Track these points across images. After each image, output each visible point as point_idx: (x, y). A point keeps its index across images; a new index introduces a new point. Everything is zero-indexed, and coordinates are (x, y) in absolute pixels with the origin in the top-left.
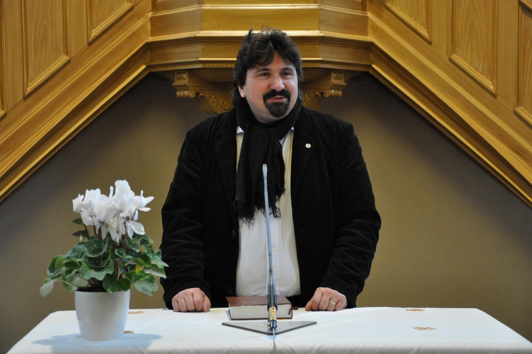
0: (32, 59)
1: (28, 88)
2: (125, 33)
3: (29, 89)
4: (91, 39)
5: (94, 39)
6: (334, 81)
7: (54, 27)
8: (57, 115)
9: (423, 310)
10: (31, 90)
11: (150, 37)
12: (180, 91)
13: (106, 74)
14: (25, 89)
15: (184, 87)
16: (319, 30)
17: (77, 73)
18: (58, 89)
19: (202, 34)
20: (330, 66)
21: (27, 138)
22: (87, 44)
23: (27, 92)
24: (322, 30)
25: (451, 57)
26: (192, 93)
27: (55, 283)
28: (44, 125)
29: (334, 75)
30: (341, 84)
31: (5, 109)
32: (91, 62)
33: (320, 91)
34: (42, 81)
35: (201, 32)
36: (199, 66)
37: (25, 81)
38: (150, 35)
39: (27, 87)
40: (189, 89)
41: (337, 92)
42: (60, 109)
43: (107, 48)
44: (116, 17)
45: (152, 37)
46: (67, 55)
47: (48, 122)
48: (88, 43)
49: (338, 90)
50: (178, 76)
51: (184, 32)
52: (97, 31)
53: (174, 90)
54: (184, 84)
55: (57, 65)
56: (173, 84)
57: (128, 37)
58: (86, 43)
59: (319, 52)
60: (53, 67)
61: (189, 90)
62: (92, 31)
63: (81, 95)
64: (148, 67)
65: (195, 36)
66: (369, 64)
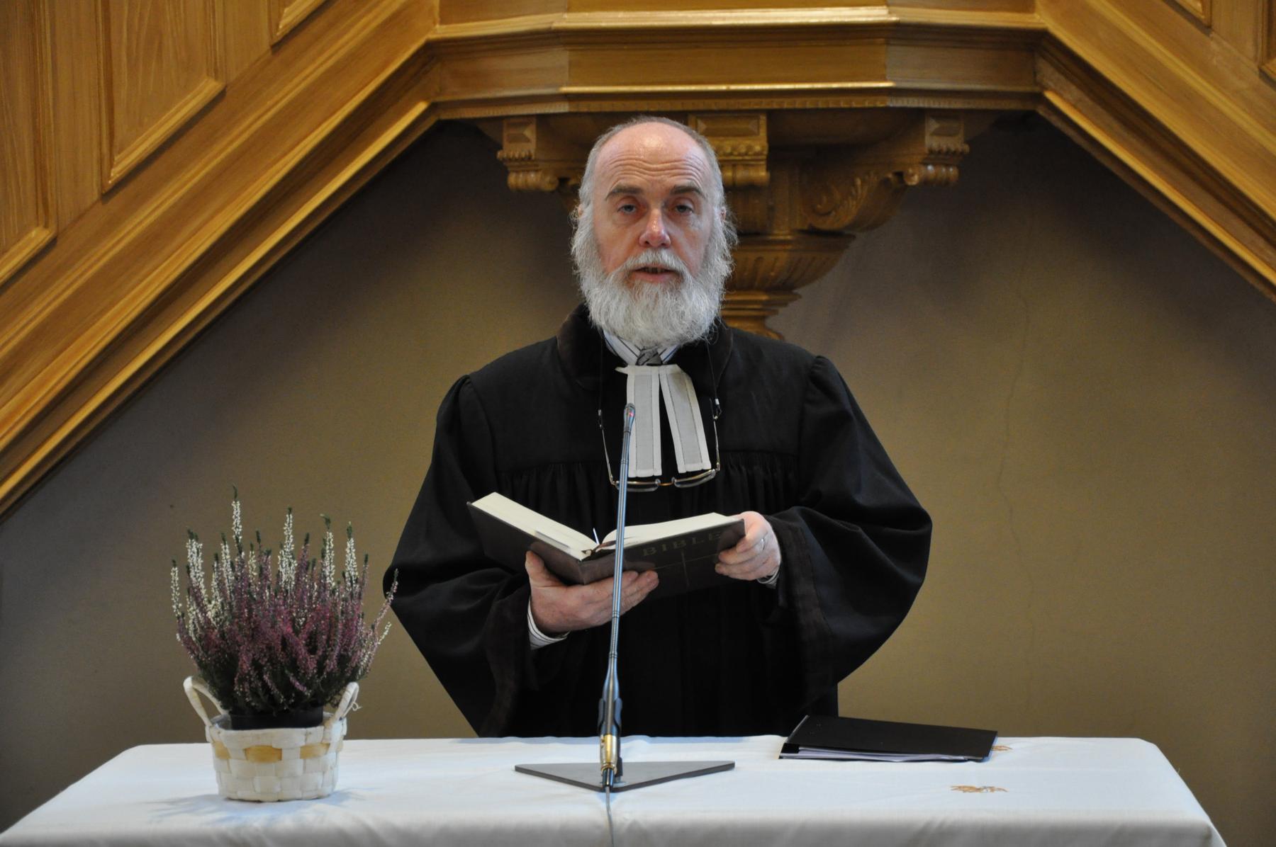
0: (121, 94)
1: (113, 170)
2: (370, 16)
3: (116, 173)
4: (279, 35)
5: (287, 32)
6: (932, 141)
7: (182, 6)
8: (189, 242)
10: (121, 174)
11: (438, 26)
12: (517, 172)
13: (320, 129)
15: (526, 163)
16: (888, 5)
17: (241, 128)
19: (569, 22)
20: (919, 103)
21: (113, 304)
22: (269, 48)
23: (110, 179)
24: (894, 5)
25: (1264, 68)
26: (548, 179)
28: (156, 268)
29: (933, 125)
30: (953, 149)
31: (53, 227)
32: (280, 95)
33: (897, 170)
34: (151, 150)
35: (566, 16)
36: (563, 108)
37: (105, 150)
38: (439, 19)
39: (111, 166)
40: (539, 168)
41: (944, 170)
43: (321, 59)
44: (31, 251)
45: (444, 27)
46: (216, 78)
47: (166, 259)
48: (272, 43)
49: (947, 166)
50: (513, 132)
51: (524, 15)
52: (297, 12)
53: (502, 169)
54: (526, 155)
55: (190, 105)
56: (499, 154)
57: (378, 26)
58: (265, 45)
59: (885, 67)
60: (178, 111)
61: (540, 170)
62: (283, 10)
63: (256, 184)
64: (433, 108)
65: (550, 28)
66: (1037, 89)
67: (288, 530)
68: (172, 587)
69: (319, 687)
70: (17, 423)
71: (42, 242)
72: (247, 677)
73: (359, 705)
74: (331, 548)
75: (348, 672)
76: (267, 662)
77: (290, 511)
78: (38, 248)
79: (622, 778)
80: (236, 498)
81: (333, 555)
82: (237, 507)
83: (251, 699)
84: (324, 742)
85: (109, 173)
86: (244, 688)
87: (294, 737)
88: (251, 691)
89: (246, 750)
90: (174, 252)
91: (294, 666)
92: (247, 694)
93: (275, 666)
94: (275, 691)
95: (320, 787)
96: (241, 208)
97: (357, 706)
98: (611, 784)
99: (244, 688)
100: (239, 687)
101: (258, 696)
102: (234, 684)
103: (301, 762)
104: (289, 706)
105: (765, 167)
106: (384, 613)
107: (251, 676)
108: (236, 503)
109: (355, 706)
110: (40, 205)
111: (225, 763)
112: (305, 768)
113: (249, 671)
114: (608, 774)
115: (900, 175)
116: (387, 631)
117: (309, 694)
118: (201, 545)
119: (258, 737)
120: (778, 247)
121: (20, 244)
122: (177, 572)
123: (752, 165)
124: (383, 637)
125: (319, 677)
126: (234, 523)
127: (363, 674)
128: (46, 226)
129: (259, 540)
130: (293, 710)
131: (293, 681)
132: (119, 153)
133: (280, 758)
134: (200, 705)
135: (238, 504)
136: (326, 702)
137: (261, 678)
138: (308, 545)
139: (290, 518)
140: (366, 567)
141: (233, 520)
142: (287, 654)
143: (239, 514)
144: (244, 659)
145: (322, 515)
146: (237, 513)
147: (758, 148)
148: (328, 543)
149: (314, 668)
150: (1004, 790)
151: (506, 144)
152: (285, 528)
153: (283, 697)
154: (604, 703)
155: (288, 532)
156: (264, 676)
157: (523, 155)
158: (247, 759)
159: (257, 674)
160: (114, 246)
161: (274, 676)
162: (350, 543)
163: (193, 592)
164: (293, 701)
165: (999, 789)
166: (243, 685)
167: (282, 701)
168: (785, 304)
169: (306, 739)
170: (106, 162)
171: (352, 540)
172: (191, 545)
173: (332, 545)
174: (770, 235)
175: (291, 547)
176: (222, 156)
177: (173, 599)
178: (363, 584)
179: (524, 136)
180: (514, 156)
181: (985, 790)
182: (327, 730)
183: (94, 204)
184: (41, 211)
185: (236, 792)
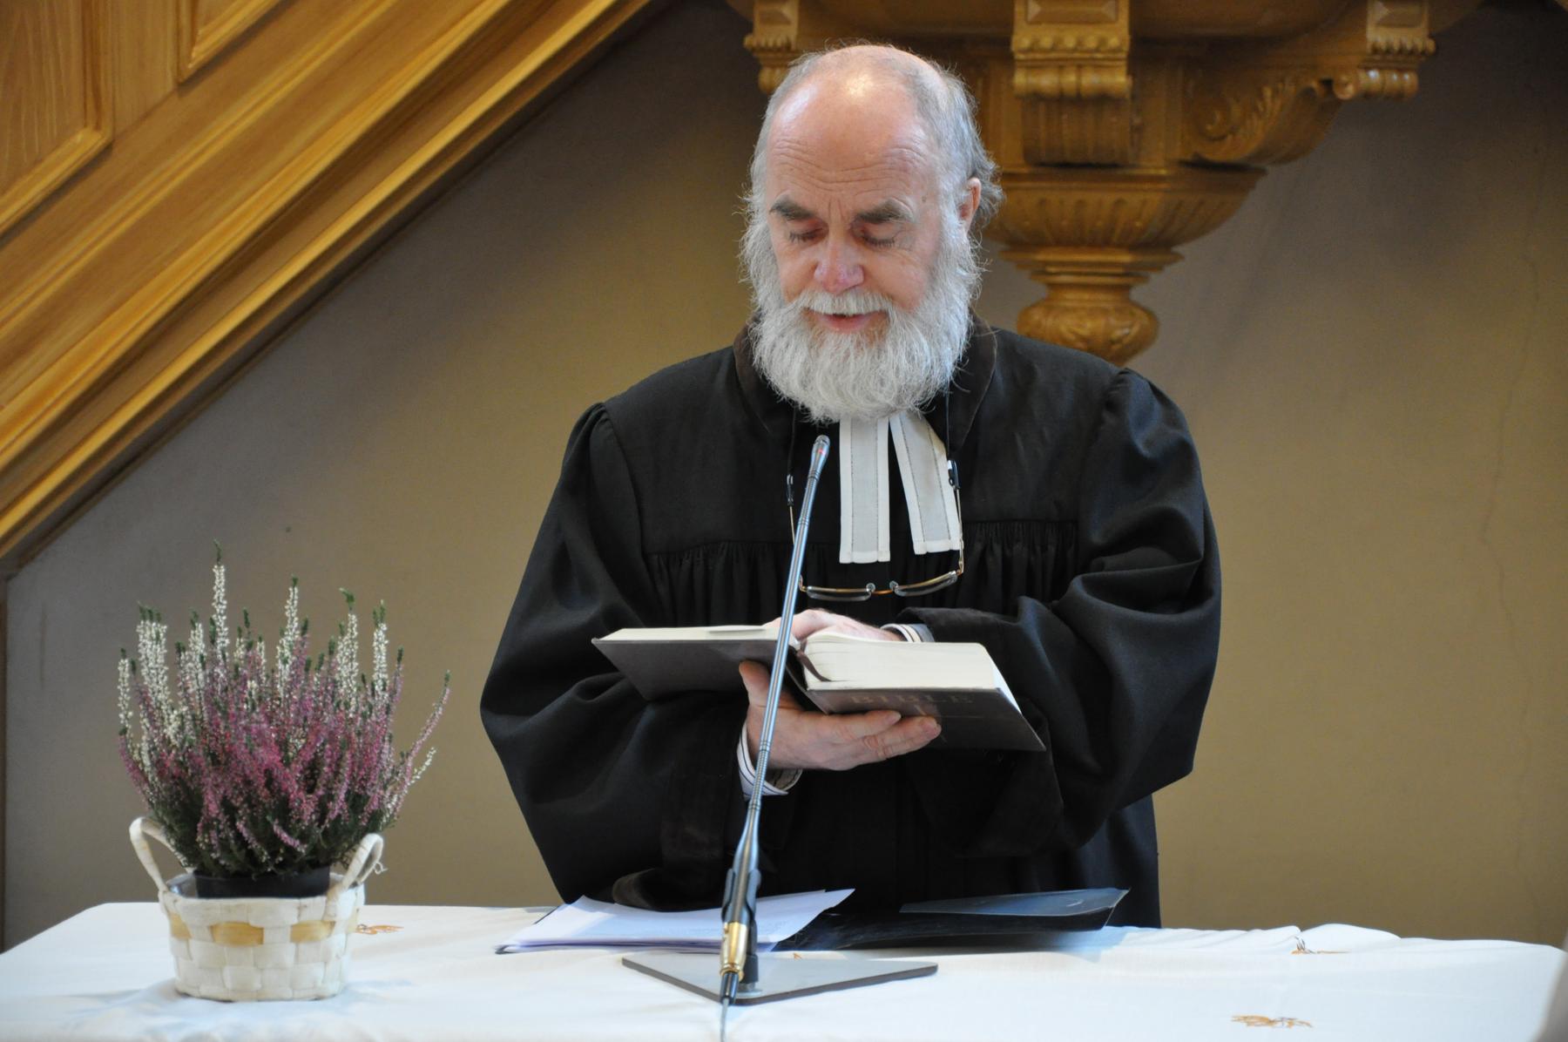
1: (195, 49)
3: (200, 53)
6: (1377, 35)
9: (930, 970)
12: (773, 67)
14: (184, 51)
18: (310, 54)
21: (189, 243)
23: (190, 62)
27: (993, 697)
30: (1409, 46)
33: (1325, 76)
37: (185, 20)
39: (193, 41)
41: (1395, 77)
42: (311, 130)
49: (1401, 71)
56: (749, 41)
67: (291, 609)
68: (119, 687)
69: (319, 840)
70: (48, 409)
71: (90, 149)
72: (215, 823)
73: (385, 866)
74: (353, 637)
75: (362, 819)
76: (243, 803)
77: (295, 582)
78: (86, 157)
79: (758, 985)
80: (219, 560)
81: (356, 647)
82: (220, 573)
83: (218, 855)
84: (327, 919)
85: (190, 52)
86: (209, 838)
87: (283, 911)
88: (219, 843)
89: (212, 928)
90: (282, 168)
91: (284, 810)
92: (215, 847)
93: (255, 809)
94: (255, 845)
95: (319, 984)
96: (376, 108)
97: (382, 867)
98: (732, 996)
99: (209, 838)
100: (204, 838)
101: (231, 851)
102: (197, 831)
103: (291, 947)
104: (276, 866)
105: (1124, 69)
106: (428, 734)
107: (219, 822)
108: (219, 569)
109: (378, 867)
110: (90, 93)
111: (184, 945)
112: (297, 956)
113: (218, 814)
114: (730, 980)
115: (1328, 84)
116: (430, 760)
117: (303, 851)
118: (165, 627)
119: (229, 909)
120: (1147, 186)
121: (59, 152)
122: (127, 665)
123: (1108, 67)
124: (424, 769)
125: (319, 826)
126: (216, 597)
127: (387, 824)
128: (97, 127)
129: (247, 623)
130: (281, 873)
131: (278, 832)
132: (206, 24)
133: (261, 941)
134: (151, 860)
135: (223, 569)
136: (335, 861)
137: (233, 826)
138: (307, 635)
139: (294, 592)
140: (399, 667)
141: (214, 593)
142: (272, 791)
143: (223, 584)
144: (210, 797)
145: (341, 589)
146: (220, 582)
147: (1114, 42)
148: (349, 630)
149: (312, 813)
150: (1308, 1025)
151: (757, 26)
152: (287, 607)
153: (266, 853)
154: (734, 874)
155: (291, 613)
156: (238, 823)
157: (779, 44)
158: (214, 940)
159: (228, 820)
160: (197, 156)
161: (253, 823)
162: (380, 634)
163: (141, 696)
164: (281, 859)
165: (1302, 1023)
166: (209, 834)
167: (264, 859)
168: (1158, 267)
169: (299, 916)
170: (186, 36)
171: (384, 627)
172: (144, 629)
173: (356, 633)
174: (1133, 166)
175: (294, 634)
176: (353, 33)
177: (120, 705)
178: (395, 692)
179: (781, 15)
180: (767, 44)
181: (1280, 1024)
182: (330, 903)
183: (166, 98)
184: (90, 105)
185: (198, 988)
